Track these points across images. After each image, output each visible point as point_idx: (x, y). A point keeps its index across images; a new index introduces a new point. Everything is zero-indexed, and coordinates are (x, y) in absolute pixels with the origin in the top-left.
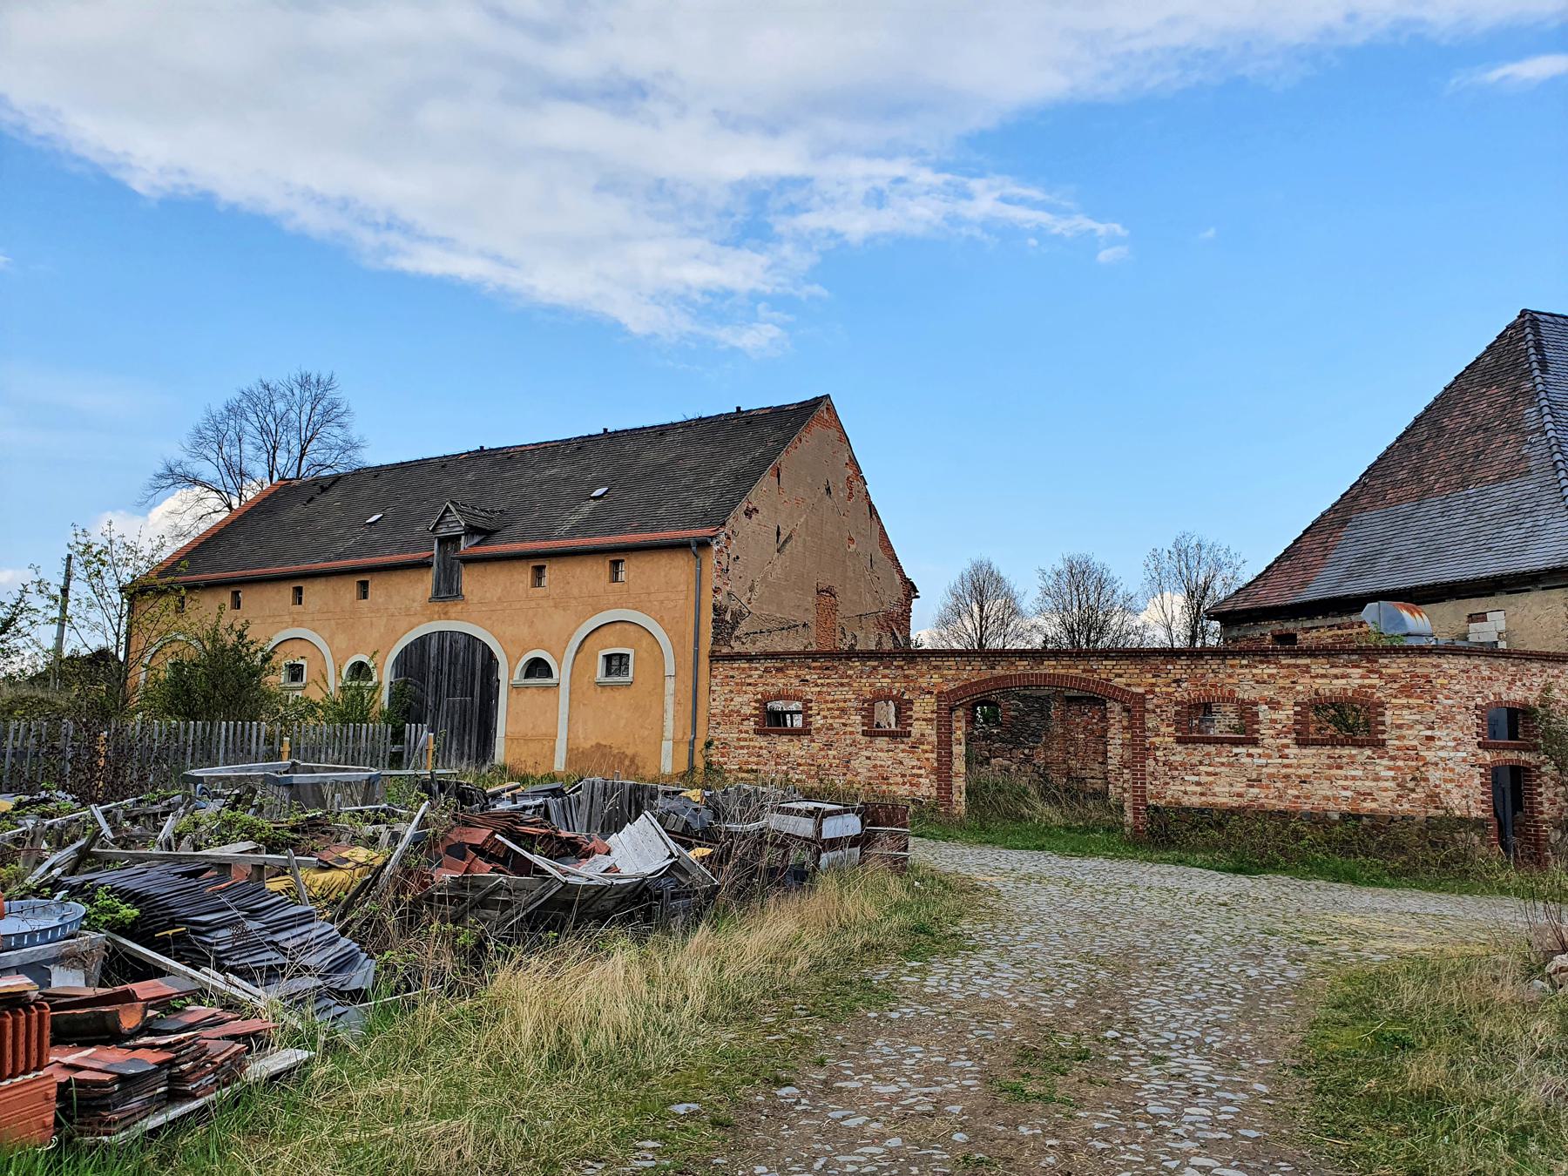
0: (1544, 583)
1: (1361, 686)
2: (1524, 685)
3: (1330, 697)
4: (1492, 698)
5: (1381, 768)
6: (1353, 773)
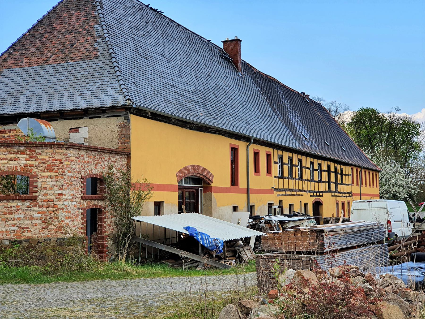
0: (108, 114)
1: (26, 165)
2: (102, 166)
3: (7, 172)
4: (88, 172)
5: (35, 212)
6: (19, 216)
